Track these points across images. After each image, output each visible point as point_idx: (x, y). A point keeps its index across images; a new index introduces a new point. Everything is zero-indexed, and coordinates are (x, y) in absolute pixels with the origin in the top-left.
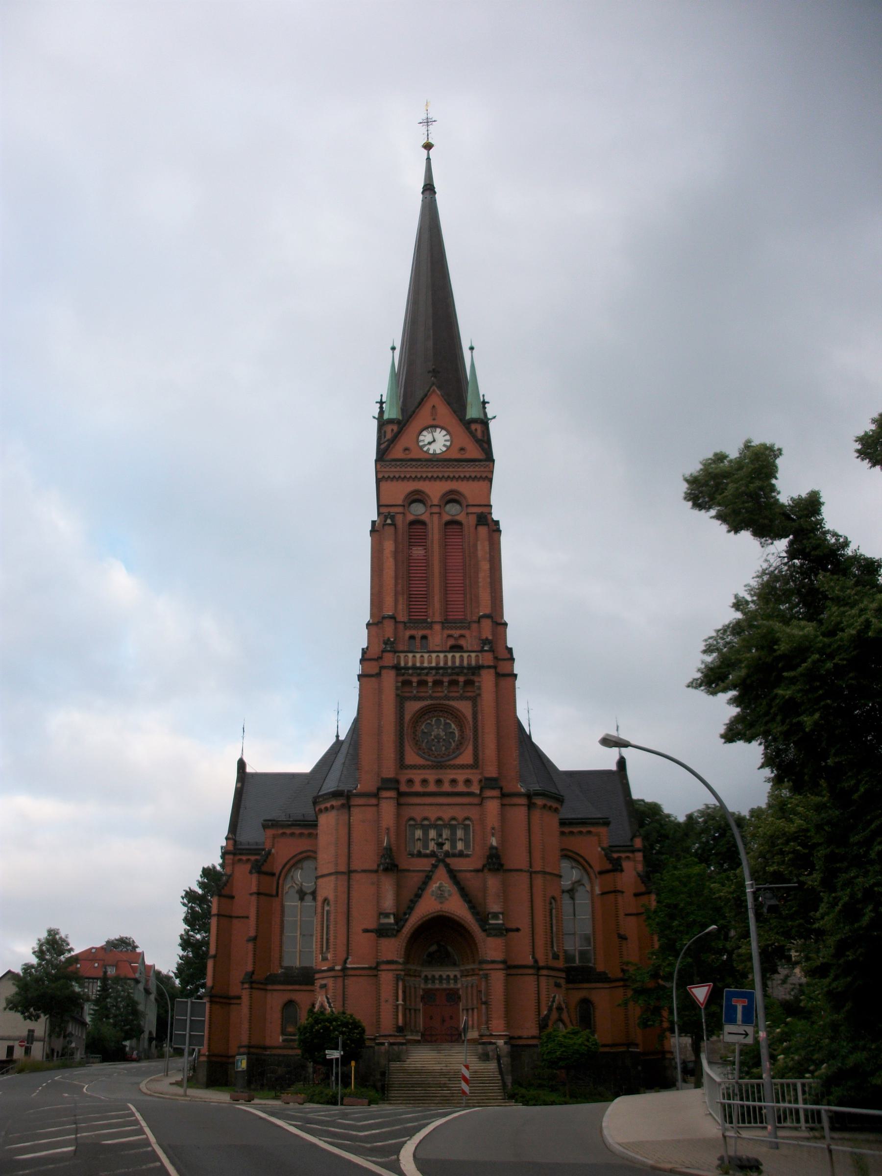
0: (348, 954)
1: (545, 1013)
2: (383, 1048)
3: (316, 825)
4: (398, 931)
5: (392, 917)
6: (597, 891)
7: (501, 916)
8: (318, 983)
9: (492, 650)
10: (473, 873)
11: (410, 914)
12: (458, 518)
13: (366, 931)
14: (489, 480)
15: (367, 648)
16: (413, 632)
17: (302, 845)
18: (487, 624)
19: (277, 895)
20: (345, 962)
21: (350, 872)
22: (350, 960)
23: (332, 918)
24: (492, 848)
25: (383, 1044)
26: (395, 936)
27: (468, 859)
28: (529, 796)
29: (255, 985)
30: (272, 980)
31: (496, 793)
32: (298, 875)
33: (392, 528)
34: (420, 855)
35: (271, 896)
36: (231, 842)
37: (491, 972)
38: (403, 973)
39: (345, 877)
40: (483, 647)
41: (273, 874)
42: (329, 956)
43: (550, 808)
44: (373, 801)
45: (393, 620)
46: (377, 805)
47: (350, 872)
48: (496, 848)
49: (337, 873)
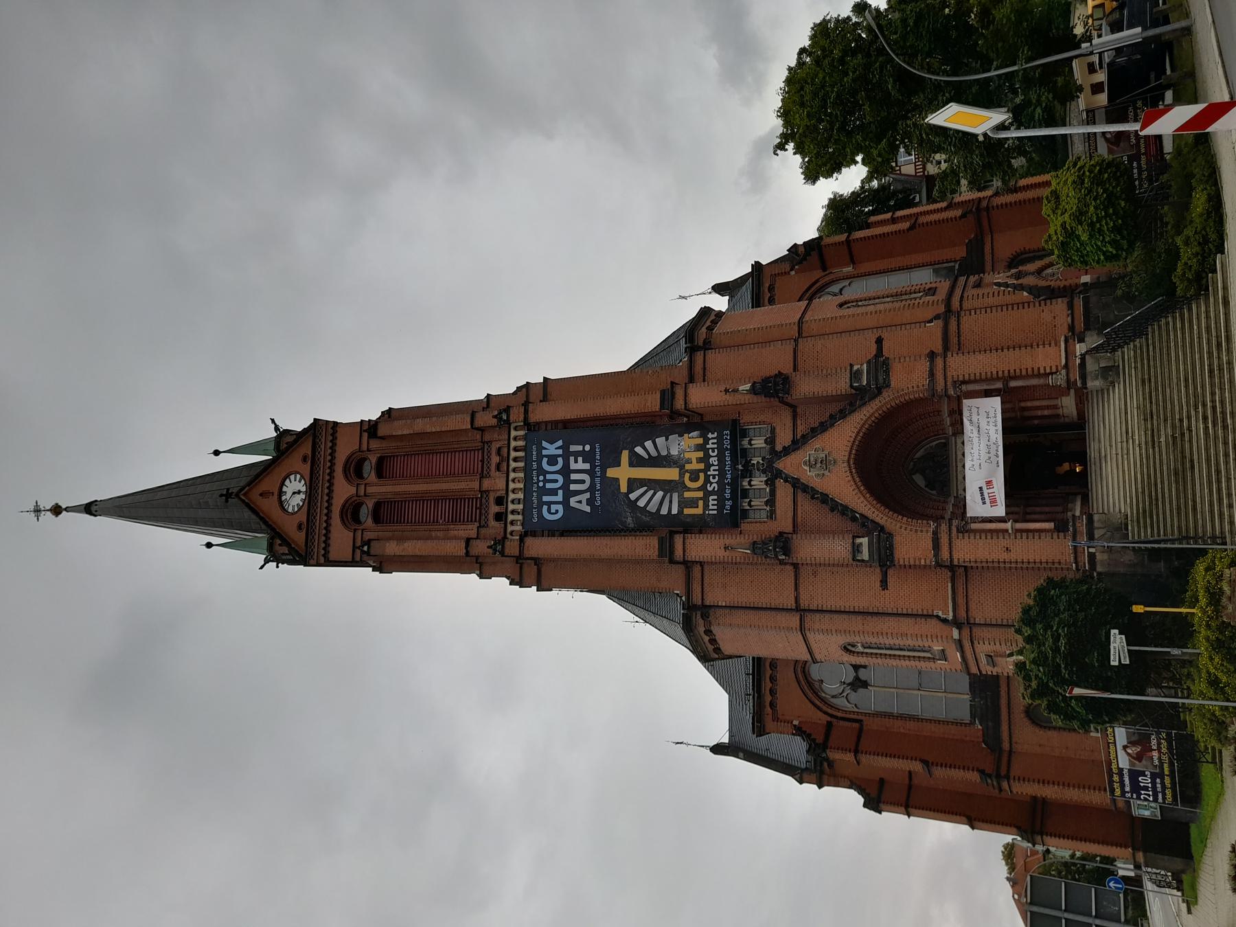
0: (931, 616)
1: (1025, 294)
2: (1099, 557)
3: (759, 659)
4: (882, 529)
5: (858, 541)
6: (849, 269)
7: (855, 368)
8: (987, 669)
10: (799, 422)
11: (853, 511)
13: (884, 584)
14: (335, 424)
15: (508, 578)
16: (491, 517)
17: (786, 679)
19: (859, 721)
20: (945, 621)
21: (800, 610)
22: (940, 614)
23: (874, 640)
25: (1092, 557)
26: (890, 535)
27: (777, 430)
29: (1003, 773)
30: (992, 740)
32: (831, 687)
33: (373, 544)
34: (771, 502)
35: (861, 730)
36: (805, 776)
37: (949, 374)
38: (955, 523)
39: (809, 617)
41: (829, 724)
42: (937, 648)
44: (696, 570)
46: (702, 564)
47: (800, 610)
49: (802, 629)
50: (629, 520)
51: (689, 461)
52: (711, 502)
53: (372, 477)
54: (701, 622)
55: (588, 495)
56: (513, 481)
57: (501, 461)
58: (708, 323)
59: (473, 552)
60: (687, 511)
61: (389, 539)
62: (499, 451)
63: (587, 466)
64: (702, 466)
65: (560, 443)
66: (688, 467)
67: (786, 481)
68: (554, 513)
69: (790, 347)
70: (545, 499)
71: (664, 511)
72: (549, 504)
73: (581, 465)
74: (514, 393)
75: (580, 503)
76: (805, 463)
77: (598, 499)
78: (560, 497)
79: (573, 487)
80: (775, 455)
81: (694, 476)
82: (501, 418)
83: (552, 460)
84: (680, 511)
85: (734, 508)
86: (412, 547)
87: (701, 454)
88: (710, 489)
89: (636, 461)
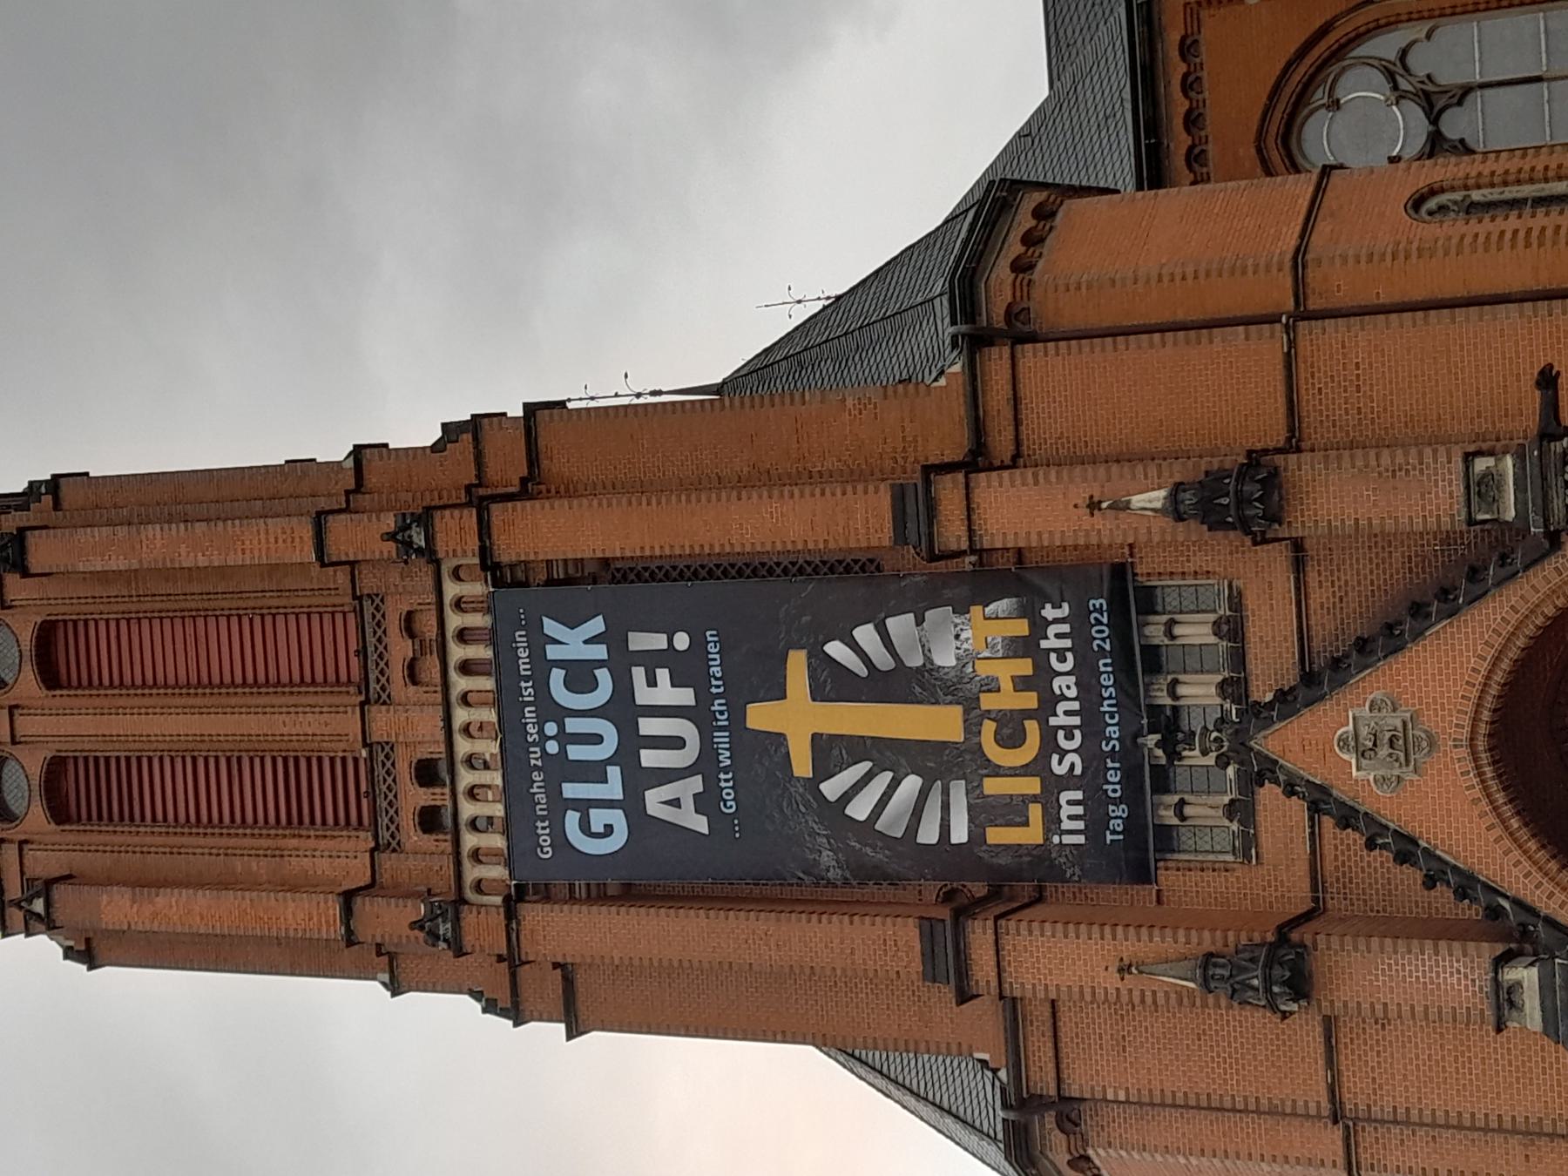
5: (1511, 974)
9: (425, 518)
10: (1312, 578)
12: (27, 637)
15: (477, 995)
16: (408, 820)
18: (348, 536)
24: (1175, 509)
27: (1250, 602)
28: (975, 342)
31: (949, 490)
33: (59, 892)
40: (419, 551)
43: (1032, 240)
45: (358, 902)
48: (1177, 489)
50: (827, 858)
51: (992, 686)
52: (1066, 811)
53: (36, 818)
54: (1058, 1138)
55: (696, 784)
56: (466, 730)
57: (422, 649)
58: (1015, 248)
59: (335, 551)
60: (997, 835)
61: (108, 881)
62: (409, 624)
63: (686, 696)
64: (1030, 700)
65: (597, 625)
66: (988, 702)
67: (1290, 791)
68: (602, 835)
69: (1271, 343)
70: (571, 790)
71: (928, 834)
72: (584, 806)
73: (666, 693)
74: (436, 447)
75: (676, 805)
76: (1343, 742)
77: (728, 793)
78: (613, 787)
79: (649, 758)
80: (1249, 713)
81: (1011, 730)
82: (408, 544)
83: (581, 677)
84: (977, 836)
85: (1134, 825)
86: (173, 909)
87: (1025, 667)
88: (1060, 770)
89: (832, 684)
